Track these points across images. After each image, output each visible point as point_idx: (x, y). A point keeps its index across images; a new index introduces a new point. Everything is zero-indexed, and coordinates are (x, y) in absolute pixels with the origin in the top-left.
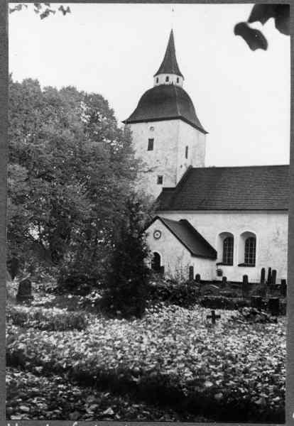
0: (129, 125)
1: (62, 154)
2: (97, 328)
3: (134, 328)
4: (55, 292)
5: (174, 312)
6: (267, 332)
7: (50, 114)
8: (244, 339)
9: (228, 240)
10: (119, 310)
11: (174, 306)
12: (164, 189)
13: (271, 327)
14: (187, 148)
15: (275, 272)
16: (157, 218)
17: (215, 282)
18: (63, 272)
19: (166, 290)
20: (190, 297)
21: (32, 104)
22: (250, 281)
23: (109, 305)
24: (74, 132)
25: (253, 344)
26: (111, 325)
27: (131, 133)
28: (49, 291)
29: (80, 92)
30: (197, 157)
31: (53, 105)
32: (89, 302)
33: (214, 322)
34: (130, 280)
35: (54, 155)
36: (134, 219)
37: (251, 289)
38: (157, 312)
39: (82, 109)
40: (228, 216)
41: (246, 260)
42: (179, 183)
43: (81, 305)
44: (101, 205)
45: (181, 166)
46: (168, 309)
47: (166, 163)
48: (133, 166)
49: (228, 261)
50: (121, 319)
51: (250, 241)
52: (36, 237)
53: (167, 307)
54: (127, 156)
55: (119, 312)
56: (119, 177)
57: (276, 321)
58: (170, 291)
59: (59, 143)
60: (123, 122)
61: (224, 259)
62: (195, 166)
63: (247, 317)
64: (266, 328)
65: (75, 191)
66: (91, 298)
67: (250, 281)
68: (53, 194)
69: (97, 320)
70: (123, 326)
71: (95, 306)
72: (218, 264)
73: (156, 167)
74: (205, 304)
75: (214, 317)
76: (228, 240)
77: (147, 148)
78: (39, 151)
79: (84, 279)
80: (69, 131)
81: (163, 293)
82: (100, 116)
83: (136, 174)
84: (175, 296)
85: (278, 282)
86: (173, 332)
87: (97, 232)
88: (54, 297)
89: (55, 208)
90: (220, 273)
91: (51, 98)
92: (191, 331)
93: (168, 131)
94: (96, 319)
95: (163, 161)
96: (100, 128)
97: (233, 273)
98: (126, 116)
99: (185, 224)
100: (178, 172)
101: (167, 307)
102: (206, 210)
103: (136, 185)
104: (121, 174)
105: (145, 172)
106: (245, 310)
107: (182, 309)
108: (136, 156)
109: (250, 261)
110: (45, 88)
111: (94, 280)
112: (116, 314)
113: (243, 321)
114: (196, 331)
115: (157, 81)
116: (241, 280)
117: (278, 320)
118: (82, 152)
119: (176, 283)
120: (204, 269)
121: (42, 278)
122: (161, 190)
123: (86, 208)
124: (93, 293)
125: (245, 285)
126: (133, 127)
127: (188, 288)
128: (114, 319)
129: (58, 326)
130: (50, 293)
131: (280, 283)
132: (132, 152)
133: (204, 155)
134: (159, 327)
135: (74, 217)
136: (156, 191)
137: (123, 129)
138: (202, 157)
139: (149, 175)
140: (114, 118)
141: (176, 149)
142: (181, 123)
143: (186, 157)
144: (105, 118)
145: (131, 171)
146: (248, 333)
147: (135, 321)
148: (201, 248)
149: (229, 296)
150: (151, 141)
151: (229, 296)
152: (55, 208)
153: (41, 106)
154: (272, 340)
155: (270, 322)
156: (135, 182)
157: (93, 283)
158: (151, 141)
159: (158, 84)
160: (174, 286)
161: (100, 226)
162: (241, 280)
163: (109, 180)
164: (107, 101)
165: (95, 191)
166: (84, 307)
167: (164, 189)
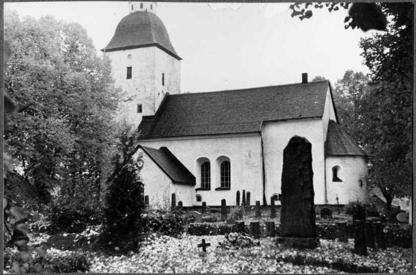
0: (108, 53)
1: (44, 86)
2: (99, 267)
3: (133, 263)
4: (49, 231)
5: (165, 242)
6: (254, 256)
7: (30, 45)
8: (236, 266)
9: (205, 166)
10: (117, 246)
11: (165, 236)
12: (144, 117)
13: (255, 250)
14: (163, 75)
15: (249, 194)
16: (139, 147)
17: (195, 208)
18: (55, 210)
19: (156, 221)
20: (178, 226)
21: (11, 35)
22: (227, 204)
23: (108, 242)
24: (55, 62)
25: (245, 270)
26: (112, 263)
27: (110, 62)
28: (43, 230)
29: (58, 21)
30: (172, 83)
31: (32, 35)
32: (84, 239)
33: (204, 250)
34: (126, 215)
35: (35, 87)
36: (128, 152)
37: (229, 212)
38: (151, 244)
39: (62, 38)
40: (203, 141)
41: (222, 184)
42: (158, 111)
43: (77, 243)
44: (85, 136)
45: (159, 94)
46: (160, 240)
47: (145, 91)
48: (113, 95)
49: (206, 186)
50: (120, 256)
51: (225, 166)
52: (22, 173)
53: (159, 237)
54: (107, 86)
55: (117, 248)
56: (101, 108)
57: (259, 244)
58: (160, 222)
59: (40, 76)
60: (103, 50)
61: (203, 185)
62: (171, 93)
63: (234, 243)
64: (252, 252)
65: (57, 127)
66: (87, 235)
67: (227, 204)
68: (36, 128)
69: (96, 259)
70: (124, 262)
71: (91, 242)
72: (197, 190)
73: (136, 96)
74: (193, 231)
75: (204, 245)
76: (205, 166)
77: (126, 76)
78: (20, 84)
79: (77, 216)
80: (49, 61)
81: (154, 224)
82: (80, 45)
83: (117, 104)
84: (164, 226)
85: (253, 203)
86: (171, 265)
87: (81, 164)
88: (48, 237)
89: (39, 142)
90: (199, 199)
91: (30, 28)
92: (187, 262)
93: (140, 58)
94: (96, 258)
95: (142, 90)
96: (80, 57)
97: (212, 198)
98: (104, 45)
99: (165, 151)
100: (156, 100)
101: (159, 237)
102: (185, 136)
103: (117, 115)
104: (103, 104)
105: (125, 101)
106: (231, 236)
107: (173, 238)
108: (116, 85)
109: (225, 184)
110: (24, 18)
111: (87, 216)
112: (115, 251)
113: (230, 246)
114: (192, 262)
115: (132, 9)
116: (220, 204)
117: (261, 242)
118: (63, 84)
119: (164, 213)
120: (186, 196)
121: (32, 216)
122: (141, 119)
123: (68, 141)
124: (88, 229)
125: (224, 208)
126: (113, 55)
127: (176, 218)
128: (113, 256)
129: (62, 269)
130: (43, 232)
131: (255, 204)
132: (110, 81)
133: (180, 82)
134: (157, 261)
135: (58, 151)
136: (135, 120)
137: (102, 58)
138: (177, 83)
139: (129, 104)
140: (93, 47)
141: (153, 77)
142: (156, 49)
143: (163, 84)
144: (85, 47)
145: (112, 101)
146: (238, 260)
147: (134, 256)
148: (182, 176)
149: (210, 220)
150: (129, 69)
151: (210, 220)
152: (39, 142)
153: (21, 36)
154: (261, 264)
155: (254, 245)
156: (117, 112)
157: (87, 218)
158: (129, 69)
159: (133, 11)
160: (163, 216)
161: (84, 157)
162: (220, 204)
163: (91, 111)
164: (361, 73)
165: (77, 123)
166: (81, 244)
167: (144, 117)
